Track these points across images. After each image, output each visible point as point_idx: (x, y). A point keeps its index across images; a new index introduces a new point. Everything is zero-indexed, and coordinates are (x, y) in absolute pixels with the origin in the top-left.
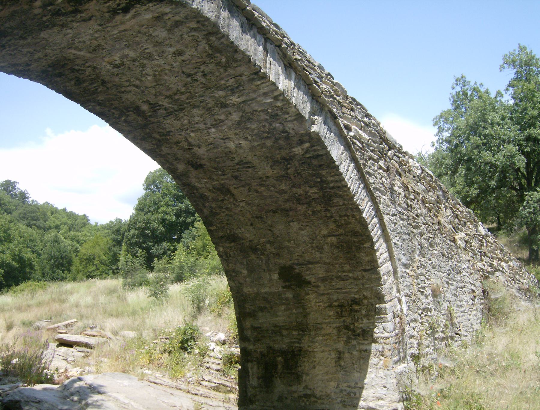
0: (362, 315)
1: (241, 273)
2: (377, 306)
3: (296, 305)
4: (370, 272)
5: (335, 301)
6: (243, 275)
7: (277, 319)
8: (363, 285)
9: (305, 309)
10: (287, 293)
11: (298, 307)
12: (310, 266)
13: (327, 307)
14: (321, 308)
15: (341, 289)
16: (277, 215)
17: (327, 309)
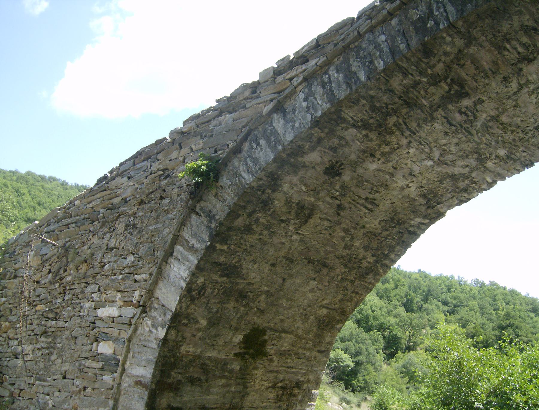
0: (297, 400)
1: (198, 322)
2: (313, 391)
3: (238, 380)
4: (323, 355)
5: (281, 381)
6: (198, 326)
7: (209, 397)
8: (312, 366)
9: (245, 387)
10: (235, 363)
11: (239, 384)
12: (284, 335)
13: (269, 387)
14: (263, 387)
15: (292, 368)
16: (310, 266)
17: (270, 390)
